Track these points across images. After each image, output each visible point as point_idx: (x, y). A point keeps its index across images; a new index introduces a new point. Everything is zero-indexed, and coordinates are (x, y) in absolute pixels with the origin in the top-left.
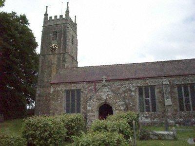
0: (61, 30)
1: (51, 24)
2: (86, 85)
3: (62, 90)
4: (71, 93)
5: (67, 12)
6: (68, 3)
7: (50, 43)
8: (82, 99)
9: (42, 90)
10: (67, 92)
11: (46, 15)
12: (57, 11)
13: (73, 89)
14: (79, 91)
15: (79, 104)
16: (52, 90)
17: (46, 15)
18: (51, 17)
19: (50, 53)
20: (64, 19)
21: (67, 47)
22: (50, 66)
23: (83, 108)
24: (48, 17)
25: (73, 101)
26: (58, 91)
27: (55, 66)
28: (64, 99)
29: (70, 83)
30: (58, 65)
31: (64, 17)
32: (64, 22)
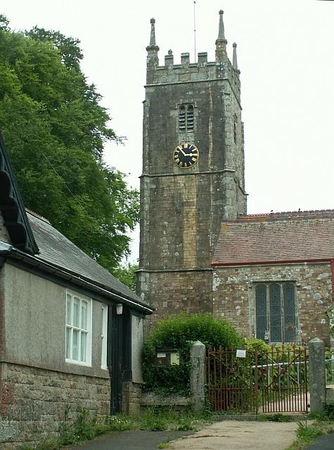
0: (196, 105)
1: (173, 79)
2: (310, 271)
3: (243, 283)
4: (268, 291)
5: (221, 42)
6: (153, 21)
7: (173, 140)
8: (299, 306)
9: (155, 280)
10: (260, 287)
11: (153, 49)
12: (187, 40)
13: (274, 279)
14: (290, 286)
15: (291, 319)
16: (216, 283)
17: (153, 49)
18: (169, 58)
19: (176, 170)
20: (210, 65)
21: (228, 154)
22: (179, 212)
23: (302, 328)
24: (161, 56)
25: (275, 308)
26: (233, 285)
27: (194, 209)
28: (252, 305)
29: (267, 264)
30: (203, 210)
31: (212, 58)
32: (212, 74)
